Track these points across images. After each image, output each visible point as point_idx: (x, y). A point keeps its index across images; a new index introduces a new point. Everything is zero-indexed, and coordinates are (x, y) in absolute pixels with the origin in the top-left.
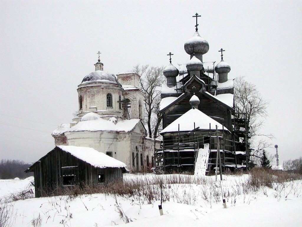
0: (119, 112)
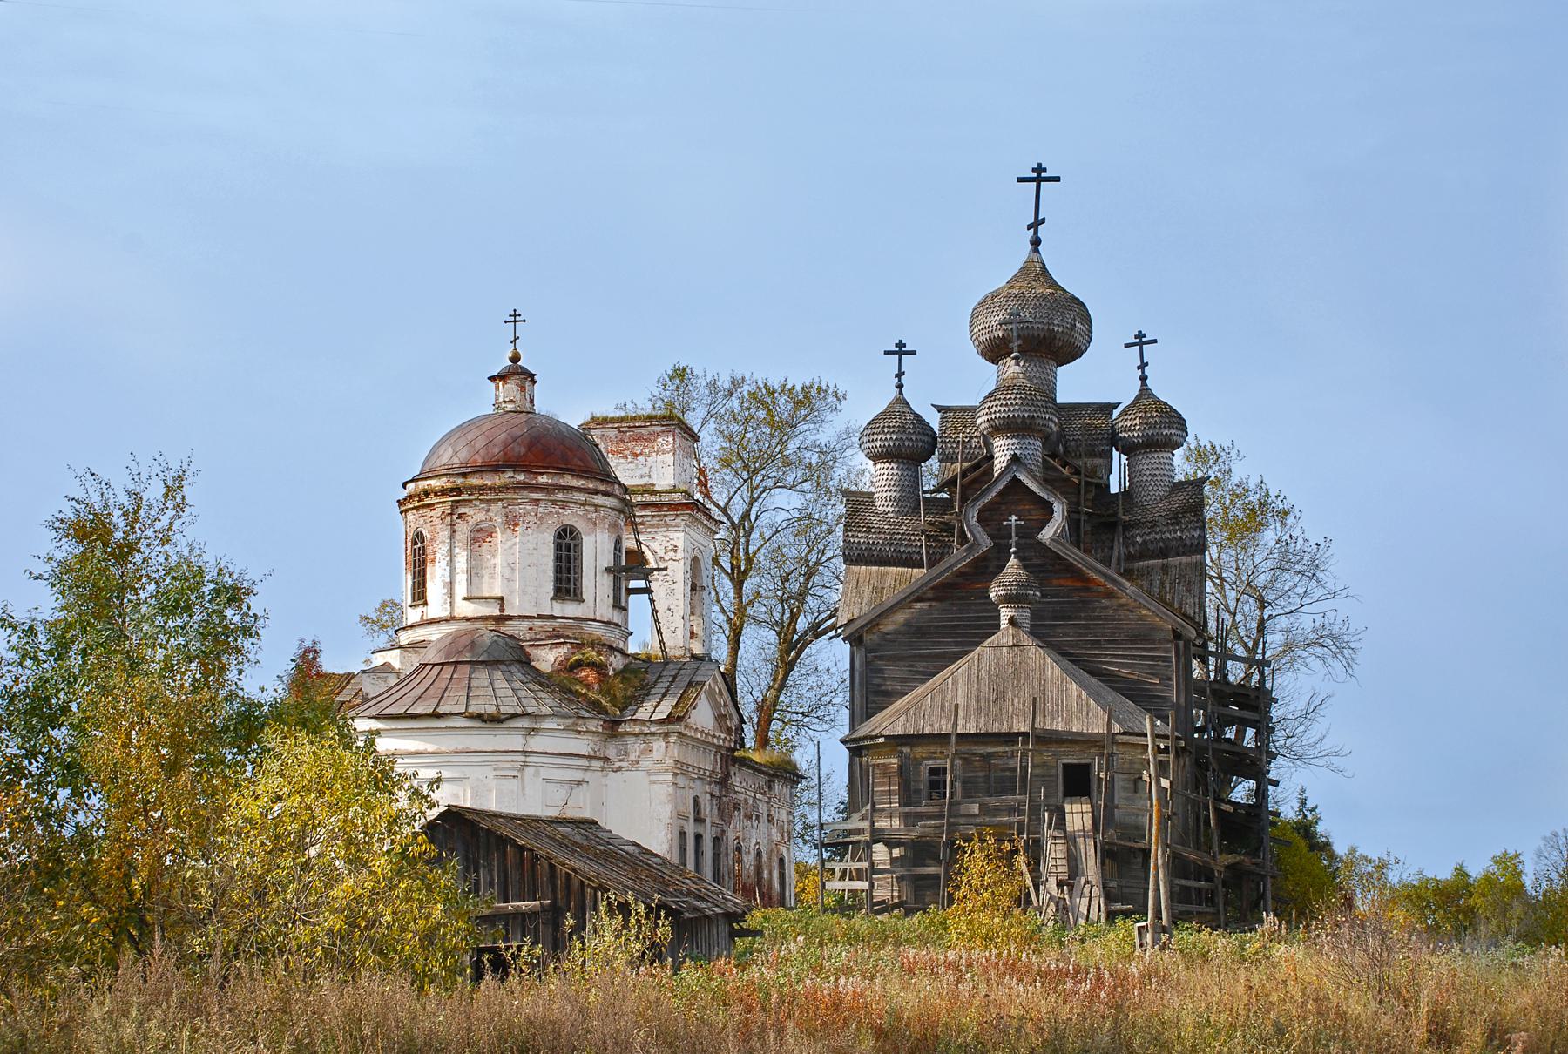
0: (608, 623)
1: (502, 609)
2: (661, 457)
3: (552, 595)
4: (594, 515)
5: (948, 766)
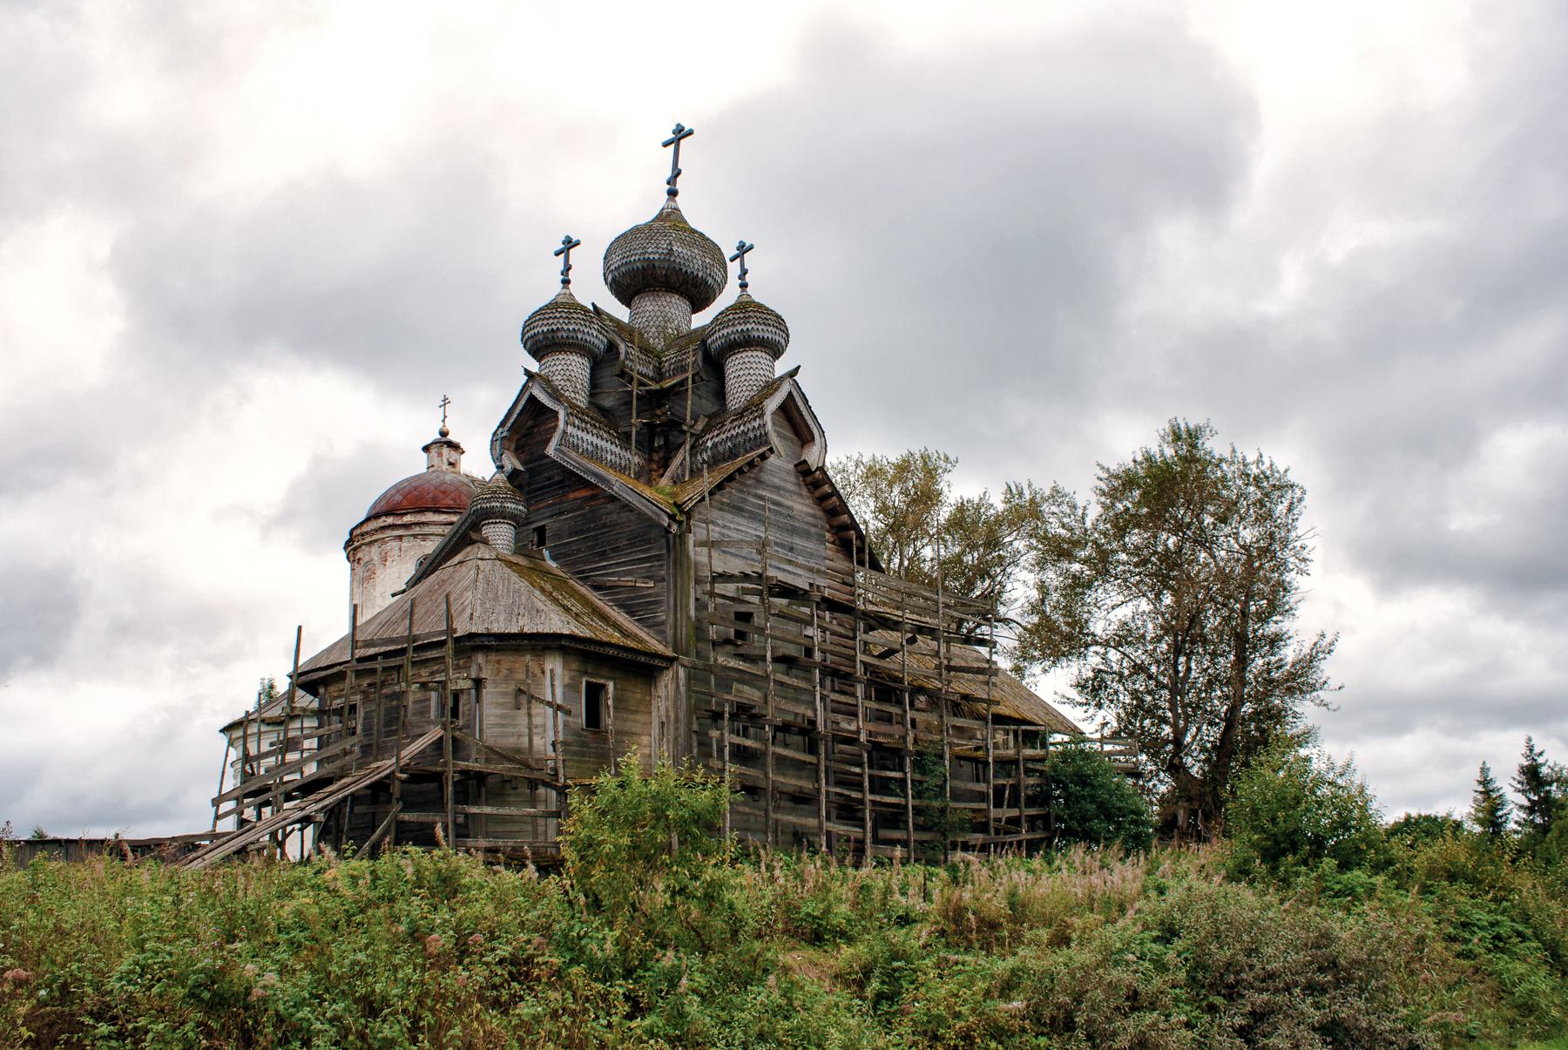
5: (991, 750)
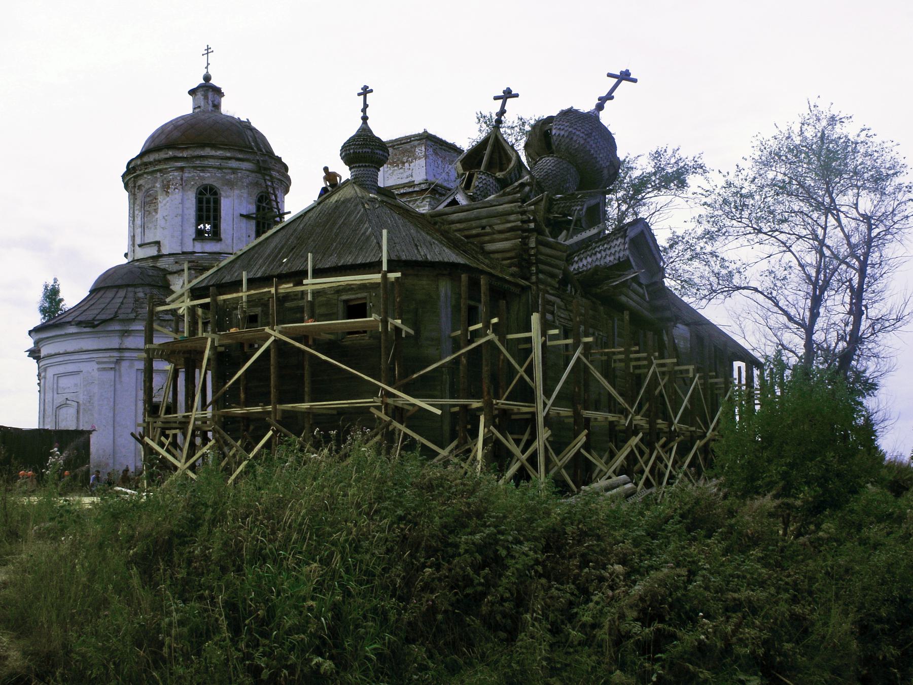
1: (159, 250)
2: (418, 162)
3: (194, 236)
4: (232, 176)
